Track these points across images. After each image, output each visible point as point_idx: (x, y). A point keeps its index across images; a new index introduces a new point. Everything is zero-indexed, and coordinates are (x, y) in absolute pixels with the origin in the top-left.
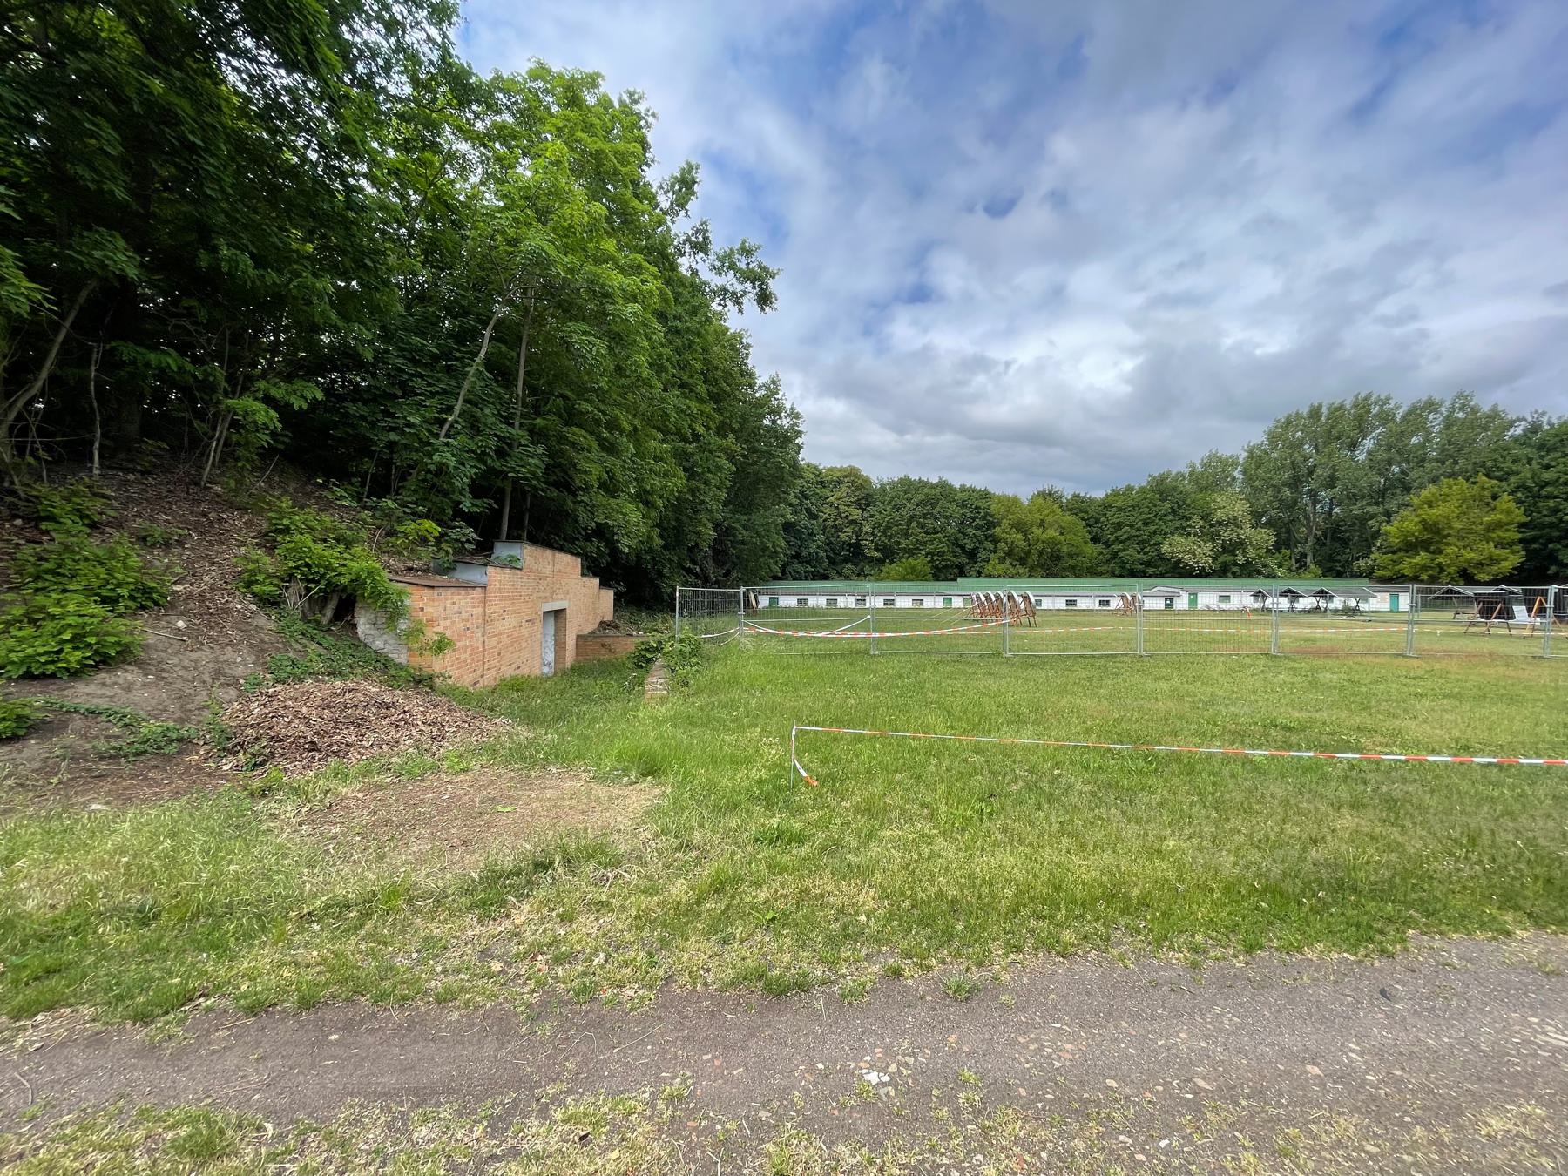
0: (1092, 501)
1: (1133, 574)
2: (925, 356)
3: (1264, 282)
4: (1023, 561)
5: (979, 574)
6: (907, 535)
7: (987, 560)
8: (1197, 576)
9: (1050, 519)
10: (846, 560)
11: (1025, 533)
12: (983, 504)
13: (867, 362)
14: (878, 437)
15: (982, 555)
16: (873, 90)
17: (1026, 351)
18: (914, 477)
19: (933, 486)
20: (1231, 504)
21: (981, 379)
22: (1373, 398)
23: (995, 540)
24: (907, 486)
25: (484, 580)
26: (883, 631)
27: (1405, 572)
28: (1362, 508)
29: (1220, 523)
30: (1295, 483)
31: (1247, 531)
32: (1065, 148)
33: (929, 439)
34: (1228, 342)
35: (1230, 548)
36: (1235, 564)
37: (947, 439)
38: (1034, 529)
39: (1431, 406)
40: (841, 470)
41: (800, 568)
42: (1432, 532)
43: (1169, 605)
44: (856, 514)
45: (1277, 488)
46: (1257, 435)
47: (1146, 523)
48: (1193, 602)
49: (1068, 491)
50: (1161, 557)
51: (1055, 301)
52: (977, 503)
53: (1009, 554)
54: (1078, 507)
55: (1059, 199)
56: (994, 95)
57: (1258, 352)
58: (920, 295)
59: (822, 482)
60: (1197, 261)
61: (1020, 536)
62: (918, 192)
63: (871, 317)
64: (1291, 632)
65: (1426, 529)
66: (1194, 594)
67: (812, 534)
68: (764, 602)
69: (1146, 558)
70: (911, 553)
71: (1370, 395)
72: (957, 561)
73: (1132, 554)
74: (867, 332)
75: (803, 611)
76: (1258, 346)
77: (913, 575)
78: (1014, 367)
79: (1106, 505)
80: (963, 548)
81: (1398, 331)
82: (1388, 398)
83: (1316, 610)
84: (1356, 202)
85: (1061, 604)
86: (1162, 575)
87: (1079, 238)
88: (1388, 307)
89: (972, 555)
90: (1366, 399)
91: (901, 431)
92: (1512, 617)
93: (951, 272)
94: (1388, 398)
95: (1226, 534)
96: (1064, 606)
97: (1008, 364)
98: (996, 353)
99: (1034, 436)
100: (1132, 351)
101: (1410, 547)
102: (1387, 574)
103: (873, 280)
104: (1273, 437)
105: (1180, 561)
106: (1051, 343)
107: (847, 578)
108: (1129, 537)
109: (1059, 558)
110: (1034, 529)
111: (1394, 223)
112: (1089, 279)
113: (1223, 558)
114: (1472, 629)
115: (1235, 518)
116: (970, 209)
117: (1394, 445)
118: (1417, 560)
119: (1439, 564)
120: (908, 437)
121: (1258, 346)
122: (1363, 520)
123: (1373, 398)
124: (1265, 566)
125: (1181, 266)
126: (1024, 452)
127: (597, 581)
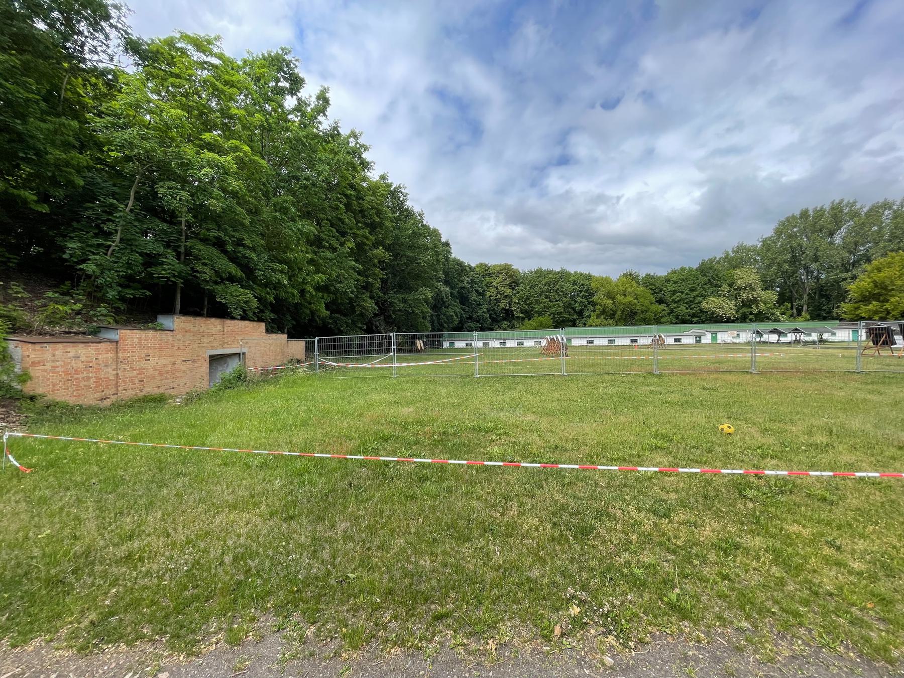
0: (658, 278)
1: (684, 322)
2: (567, 196)
3: (785, 136)
4: (612, 316)
5: (585, 325)
6: (537, 302)
7: (589, 316)
8: (725, 322)
9: (629, 290)
10: (504, 319)
11: (613, 299)
12: (586, 282)
13: (533, 202)
14: (541, 246)
15: (586, 313)
16: (530, 41)
17: (630, 191)
18: (544, 268)
19: (556, 273)
20: (748, 276)
21: (601, 208)
22: (844, 203)
23: (594, 304)
24: (540, 273)
25: (117, 338)
26: (408, 366)
27: (863, 315)
28: (837, 274)
29: (740, 288)
30: (794, 260)
31: (759, 293)
32: (650, 64)
33: (572, 246)
34: (763, 174)
35: (747, 304)
36: (751, 313)
37: (583, 244)
38: (619, 297)
39: (886, 205)
40: (500, 266)
41: (472, 325)
42: (882, 288)
43: (698, 339)
44: (508, 291)
45: (780, 265)
46: (768, 231)
47: (692, 290)
48: (714, 338)
49: (642, 273)
50: (701, 311)
51: (649, 158)
52: (583, 282)
53: (603, 312)
54: (650, 282)
55: (648, 96)
56: (605, 36)
57: (784, 179)
58: (564, 161)
59: (490, 274)
60: (739, 126)
61: (610, 301)
62: (558, 100)
63: (536, 176)
64: (781, 356)
65: (876, 286)
66: (714, 334)
67: (479, 304)
68: (480, 344)
69: (692, 312)
70: (540, 314)
71: (842, 201)
72: (571, 318)
73: (683, 309)
74: (534, 184)
75: (504, 350)
76: (783, 175)
77: (542, 326)
78: (622, 201)
79: (667, 280)
80: (574, 309)
81: (881, 160)
82: (855, 202)
83: (797, 342)
84: (847, 80)
85: (691, 340)
86: (703, 322)
87: (662, 115)
88: (874, 144)
89: (580, 313)
90: (840, 203)
91: (554, 241)
92: (894, 343)
93: (582, 146)
94: (855, 202)
95: (744, 295)
96: (629, 343)
97: (619, 198)
98: (612, 192)
99: (638, 240)
100: (700, 184)
101: (866, 299)
102: (851, 316)
103: (535, 154)
104: (779, 232)
105: (713, 313)
106: (646, 184)
107: (505, 329)
108: (680, 299)
109: (635, 313)
110: (619, 297)
111: (875, 91)
112: (669, 142)
113: (743, 310)
114: (866, 352)
115: (751, 284)
116: (593, 107)
117: (860, 234)
118: (871, 307)
119: (887, 309)
120: (560, 245)
121: (783, 175)
122: (837, 281)
123: (844, 203)
124: (772, 314)
125: (729, 130)
126: (631, 251)
127: (286, 336)
